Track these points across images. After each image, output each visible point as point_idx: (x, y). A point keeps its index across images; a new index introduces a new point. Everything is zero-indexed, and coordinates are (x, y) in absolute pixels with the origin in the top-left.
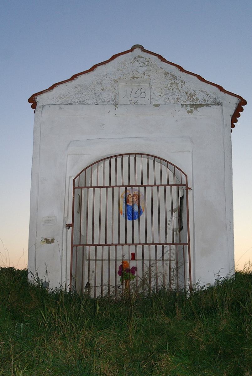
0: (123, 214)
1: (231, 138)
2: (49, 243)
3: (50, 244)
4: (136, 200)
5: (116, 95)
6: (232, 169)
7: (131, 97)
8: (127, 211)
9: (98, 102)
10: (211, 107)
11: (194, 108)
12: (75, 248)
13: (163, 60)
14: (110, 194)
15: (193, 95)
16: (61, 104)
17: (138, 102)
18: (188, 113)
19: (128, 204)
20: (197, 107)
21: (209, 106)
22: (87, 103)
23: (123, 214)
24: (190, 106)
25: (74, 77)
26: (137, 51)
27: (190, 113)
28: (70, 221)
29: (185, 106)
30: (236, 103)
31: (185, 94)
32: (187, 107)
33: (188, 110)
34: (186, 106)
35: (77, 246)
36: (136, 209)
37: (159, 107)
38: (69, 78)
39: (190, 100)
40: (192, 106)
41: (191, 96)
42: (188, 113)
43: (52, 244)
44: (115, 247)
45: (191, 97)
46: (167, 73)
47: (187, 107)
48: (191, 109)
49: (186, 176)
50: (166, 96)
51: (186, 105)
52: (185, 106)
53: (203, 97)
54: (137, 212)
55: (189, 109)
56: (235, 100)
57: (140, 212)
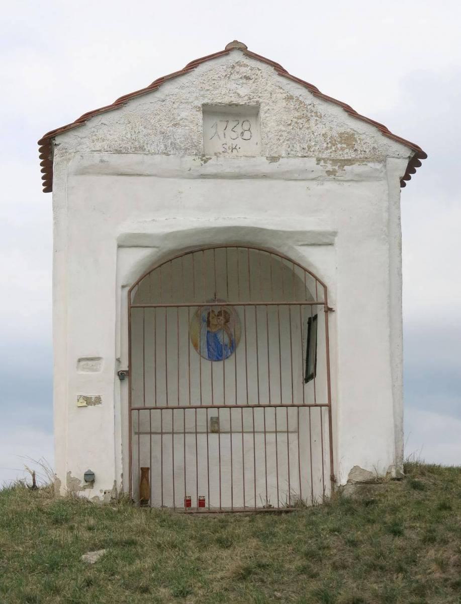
1: (400, 219)
2: (91, 405)
3: (93, 407)
6: (402, 275)
9: (168, 149)
10: (366, 165)
11: (339, 167)
13: (280, 70)
14: (282, 448)
16: (100, 151)
17: (237, 147)
18: (329, 175)
20: (343, 164)
21: (364, 163)
22: (149, 151)
24: (331, 162)
25: (122, 102)
26: (236, 56)
27: (332, 175)
28: (125, 367)
29: (322, 161)
30: (409, 157)
31: (322, 138)
32: (327, 165)
33: (327, 169)
34: (324, 163)
36: (224, 338)
37: (278, 163)
39: (331, 150)
40: (335, 161)
42: (329, 175)
43: (96, 405)
45: (332, 144)
46: (289, 98)
47: (326, 163)
48: (334, 167)
49: (325, 287)
50: (289, 142)
51: (325, 160)
52: (322, 161)
53: (300, 95)
55: (330, 167)
56: (407, 153)
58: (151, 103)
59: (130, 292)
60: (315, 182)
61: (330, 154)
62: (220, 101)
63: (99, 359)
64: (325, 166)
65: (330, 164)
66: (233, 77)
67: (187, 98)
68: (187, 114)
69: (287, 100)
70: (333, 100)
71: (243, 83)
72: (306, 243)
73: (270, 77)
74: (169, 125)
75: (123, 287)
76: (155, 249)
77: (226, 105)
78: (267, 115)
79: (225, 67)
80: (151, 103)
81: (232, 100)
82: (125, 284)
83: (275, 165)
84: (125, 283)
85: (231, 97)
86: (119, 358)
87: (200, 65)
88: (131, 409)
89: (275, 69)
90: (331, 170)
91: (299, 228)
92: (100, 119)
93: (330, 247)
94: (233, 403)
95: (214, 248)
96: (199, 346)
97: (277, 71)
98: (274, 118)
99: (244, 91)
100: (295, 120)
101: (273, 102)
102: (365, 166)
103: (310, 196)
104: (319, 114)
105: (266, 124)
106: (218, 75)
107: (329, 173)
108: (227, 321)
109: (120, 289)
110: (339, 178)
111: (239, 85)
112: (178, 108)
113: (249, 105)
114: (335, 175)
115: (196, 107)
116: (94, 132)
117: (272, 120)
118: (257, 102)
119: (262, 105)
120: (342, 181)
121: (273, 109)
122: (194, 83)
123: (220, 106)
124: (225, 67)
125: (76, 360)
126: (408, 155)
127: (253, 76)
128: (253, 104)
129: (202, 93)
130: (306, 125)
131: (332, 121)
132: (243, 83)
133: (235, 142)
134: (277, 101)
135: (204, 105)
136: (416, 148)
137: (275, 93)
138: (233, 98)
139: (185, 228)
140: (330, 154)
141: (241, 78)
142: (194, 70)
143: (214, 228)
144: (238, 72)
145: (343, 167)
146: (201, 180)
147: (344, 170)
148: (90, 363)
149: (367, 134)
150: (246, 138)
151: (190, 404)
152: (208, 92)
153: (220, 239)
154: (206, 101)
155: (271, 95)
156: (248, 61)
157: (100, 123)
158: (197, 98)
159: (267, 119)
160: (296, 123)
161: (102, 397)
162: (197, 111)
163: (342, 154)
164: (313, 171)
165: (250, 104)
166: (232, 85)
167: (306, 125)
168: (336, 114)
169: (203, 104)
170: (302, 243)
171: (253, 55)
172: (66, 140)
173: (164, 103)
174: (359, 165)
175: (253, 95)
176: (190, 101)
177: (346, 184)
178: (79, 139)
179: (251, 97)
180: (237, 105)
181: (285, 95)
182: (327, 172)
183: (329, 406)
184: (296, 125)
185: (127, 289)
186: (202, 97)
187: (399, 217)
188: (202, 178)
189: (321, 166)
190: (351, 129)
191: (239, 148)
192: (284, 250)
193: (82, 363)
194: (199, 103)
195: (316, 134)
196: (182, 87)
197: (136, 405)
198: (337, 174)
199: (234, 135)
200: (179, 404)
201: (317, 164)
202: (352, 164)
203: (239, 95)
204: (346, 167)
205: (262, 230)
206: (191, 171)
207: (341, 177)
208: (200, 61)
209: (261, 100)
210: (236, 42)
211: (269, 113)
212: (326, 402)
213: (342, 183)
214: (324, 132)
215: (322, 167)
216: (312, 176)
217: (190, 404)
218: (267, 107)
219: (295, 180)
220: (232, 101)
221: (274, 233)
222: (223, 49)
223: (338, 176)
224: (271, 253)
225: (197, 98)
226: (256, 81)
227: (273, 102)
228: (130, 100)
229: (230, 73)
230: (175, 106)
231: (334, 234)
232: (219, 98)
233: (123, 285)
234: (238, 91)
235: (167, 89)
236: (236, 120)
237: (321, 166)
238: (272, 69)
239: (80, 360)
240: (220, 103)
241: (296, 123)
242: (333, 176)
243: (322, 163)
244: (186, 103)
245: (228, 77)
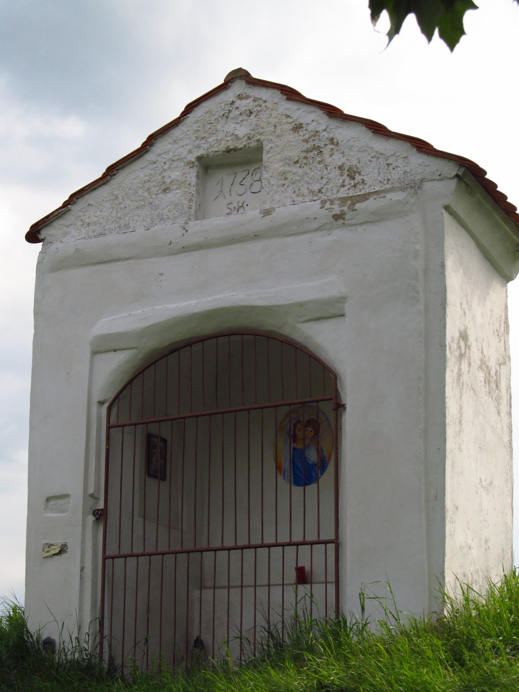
0: (283, 472)
4: (312, 434)
5: (191, 199)
7: (231, 195)
8: (293, 463)
10: (384, 197)
12: (109, 562)
15: (355, 172)
17: (245, 205)
18: (336, 220)
19: (295, 445)
21: (381, 195)
23: (283, 472)
24: (339, 202)
27: (340, 219)
29: (328, 203)
33: (334, 213)
34: (330, 204)
35: (113, 558)
36: (312, 456)
38: (100, 175)
41: (352, 173)
42: (336, 220)
44: (161, 558)
48: (342, 209)
52: (328, 203)
54: (315, 464)
55: (337, 210)
57: (323, 465)
58: (142, 168)
59: (109, 409)
60: (320, 233)
61: (347, 192)
62: (216, 150)
63: (66, 496)
64: (330, 208)
65: (338, 205)
66: (231, 115)
67: (179, 154)
68: (148, 171)
69: (295, 131)
70: (353, 118)
71: (242, 121)
72: (309, 318)
73: (276, 105)
74: (159, 192)
75: (101, 403)
76: (133, 351)
77: (224, 152)
78: (269, 155)
79: (223, 105)
80: (142, 168)
81: (229, 145)
82: (102, 400)
83: (268, 218)
84: (102, 399)
85: (228, 141)
86: (93, 494)
87: (195, 109)
88: (105, 558)
89: (281, 93)
90: (339, 213)
91: (296, 298)
92: (85, 200)
93: (342, 317)
94: (232, 544)
95: (202, 340)
96: (283, 469)
97: (286, 94)
98: (278, 157)
99: (242, 131)
100: (304, 154)
101: (278, 136)
102: (382, 199)
103: (313, 253)
104: (335, 141)
105: (268, 167)
106: (215, 117)
107: (336, 217)
108: (317, 432)
109: (95, 407)
110: (350, 221)
111: (238, 123)
112: (170, 168)
113: (249, 147)
114: (344, 219)
115: (189, 163)
116: (80, 216)
117: (275, 161)
118: (258, 140)
119: (265, 143)
120: (355, 225)
121: (277, 146)
122: (188, 133)
123: (218, 155)
124: (223, 105)
125: (45, 499)
126: (455, 173)
127: (255, 109)
128: (253, 144)
129: (197, 143)
130: (319, 159)
131: (352, 146)
132: (242, 121)
133: (241, 199)
134: (282, 135)
135: (199, 159)
136: (462, 161)
137: (281, 125)
138: (230, 142)
139: (161, 320)
140: (347, 192)
141: (241, 114)
142: (188, 117)
143: (195, 314)
144: (237, 108)
145: (354, 205)
146: (184, 254)
147: (356, 210)
148: (59, 502)
149: (397, 154)
150: (256, 191)
151: (169, 548)
152: (203, 141)
153: (209, 328)
154: (200, 152)
155: (275, 128)
156: (251, 90)
157: (87, 204)
158: (190, 152)
159: (270, 160)
160: (306, 158)
161: (68, 545)
162: (190, 167)
163: (364, 188)
164: (315, 218)
165: (251, 145)
166: (230, 126)
167: (319, 159)
168: (358, 136)
169: (197, 157)
170: (304, 319)
171: (256, 81)
172: (50, 232)
173: (154, 166)
174: (374, 199)
175: (253, 133)
176: (183, 156)
177: (360, 229)
178: (65, 228)
179: (251, 136)
180: (235, 150)
181: (293, 124)
182: (334, 216)
183: (337, 542)
184: (305, 161)
185: (107, 405)
186: (196, 149)
187: (442, 263)
188: (185, 252)
189: (326, 209)
190: (376, 152)
191: (247, 205)
192: (287, 331)
193: (51, 503)
194: (192, 158)
195: (329, 168)
196: (175, 142)
197: (112, 550)
198: (347, 217)
199: (241, 191)
200: (119, 552)
201: (322, 208)
202: (367, 199)
203: (237, 136)
204: (357, 206)
205: (252, 308)
206: (172, 245)
207: (351, 220)
208: (194, 104)
209: (262, 137)
210: (240, 69)
211: (272, 152)
212: (332, 537)
213: (354, 228)
214: (340, 164)
215: (327, 211)
216: (315, 225)
217: (169, 548)
218: (270, 145)
219: (294, 234)
220: (229, 146)
221: (268, 310)
222: (222, 82)
223: (348, 220)
224: (242, 334)
225: (190, 152)
226: (259, 114)
227: (278, 136)
228: (119, 169)
229: (228, 112)
230: (166, 167)
231: (343, 299)
232: (216, 145)
233: (99, 400)
234: (237, 133)
235: (161, 146)
236: (246, 170)
237: (326, 209)
238: (278, 93)
239: (48, 500)
240: (216, 152)
241: (306, 158)
242: (341, 221)
243: (328, 205)
244: (178, 159)
245: (226, 116)
